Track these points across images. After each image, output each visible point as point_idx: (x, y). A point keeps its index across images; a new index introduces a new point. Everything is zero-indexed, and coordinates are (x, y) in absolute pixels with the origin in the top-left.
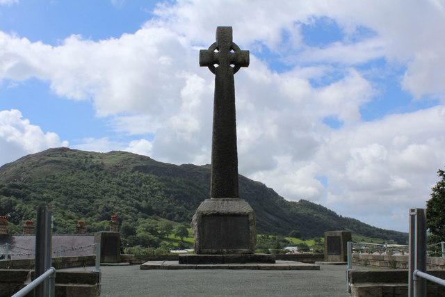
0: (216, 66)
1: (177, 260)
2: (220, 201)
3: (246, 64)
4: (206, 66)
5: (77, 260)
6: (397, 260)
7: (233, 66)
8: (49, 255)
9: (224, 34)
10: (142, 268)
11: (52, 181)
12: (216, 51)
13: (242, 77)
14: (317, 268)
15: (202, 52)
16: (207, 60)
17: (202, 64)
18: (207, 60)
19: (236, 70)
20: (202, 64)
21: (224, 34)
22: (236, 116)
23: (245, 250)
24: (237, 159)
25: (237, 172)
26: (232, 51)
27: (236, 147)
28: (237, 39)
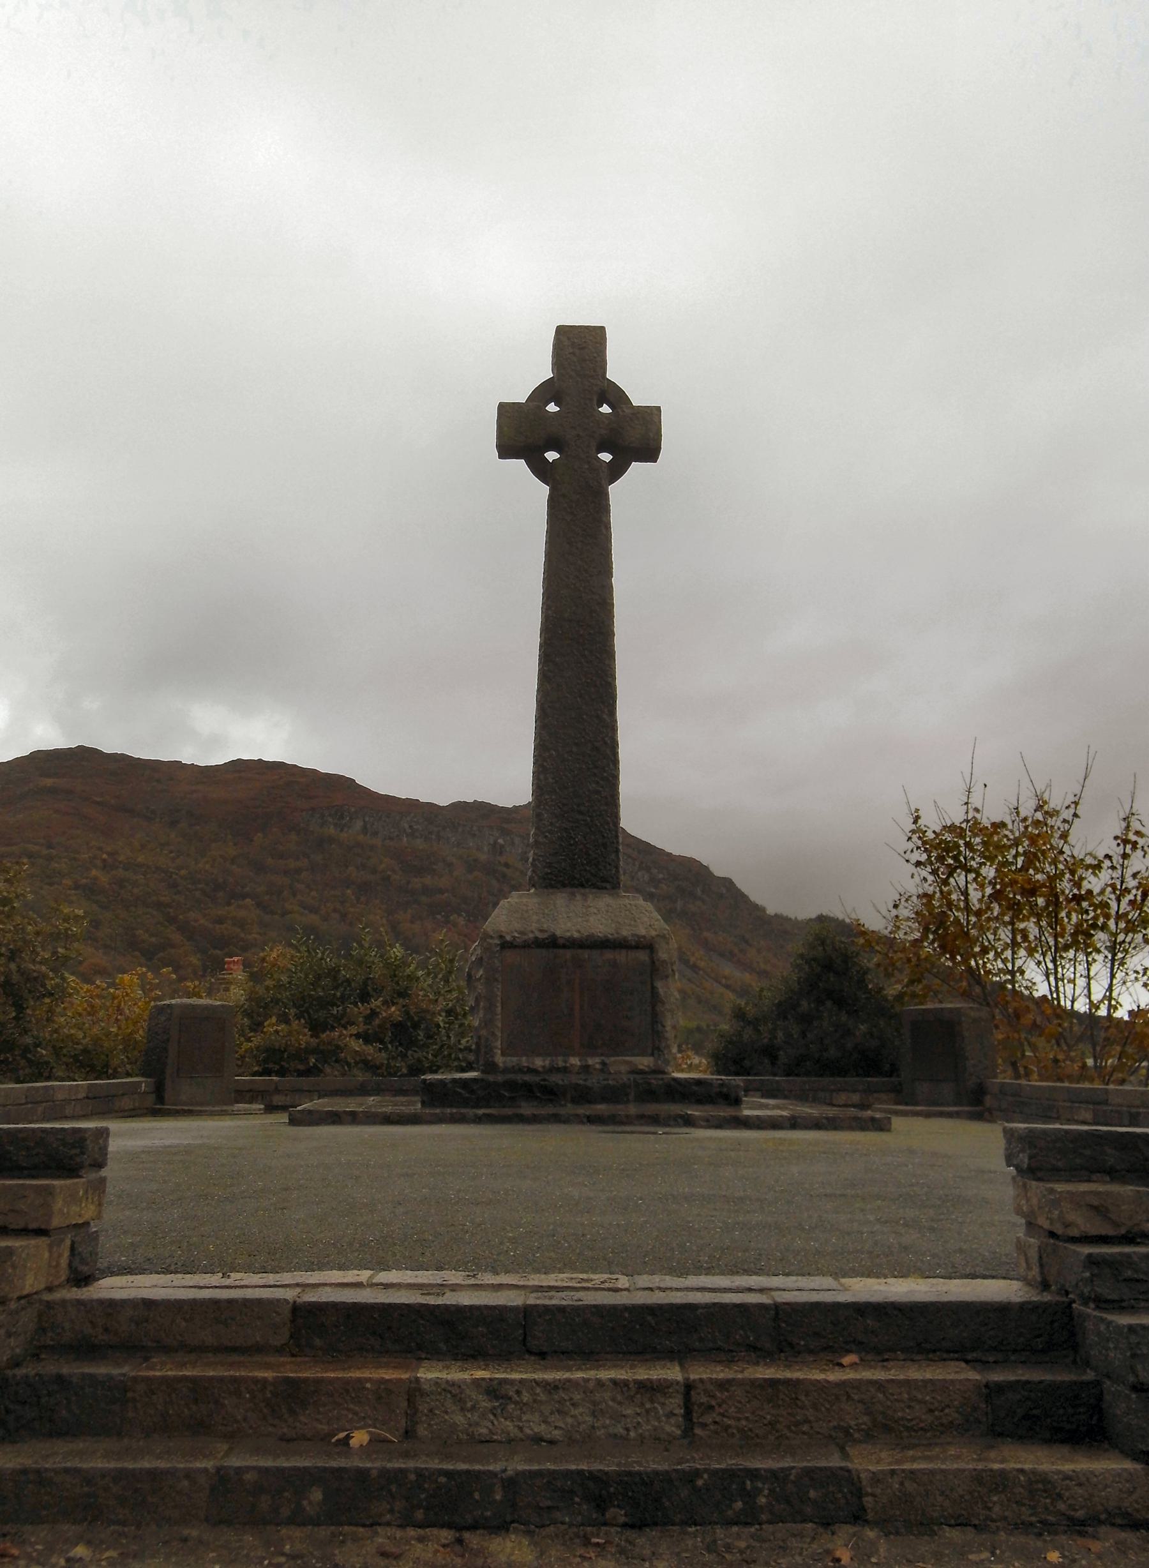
0: (552, 456)
1: (416, 1093)
2: (560, 899)
3: (650, 451)
4: (517, 456)
5: (81, 1095)
6: (892, 1095)
7: (606, 457)
8: (897, 1113)
9: (580, 349)
10: (293, 1122)
11: (45, 852)
12: (552, 408)
13: (630, 495)
14: (880, 1126)
15: (504, 410)
16: (522, 433)
17: (506, 450)
18: (522, 433)
19: (616, 470)
20: (506, 450)
21: (580, 349)
22: (617, 640)
23: (644, 1062)
24: (615, 762)
25: (616, 817)
26: (605, 409)
27: (614, 746)
28: (619, 369)
